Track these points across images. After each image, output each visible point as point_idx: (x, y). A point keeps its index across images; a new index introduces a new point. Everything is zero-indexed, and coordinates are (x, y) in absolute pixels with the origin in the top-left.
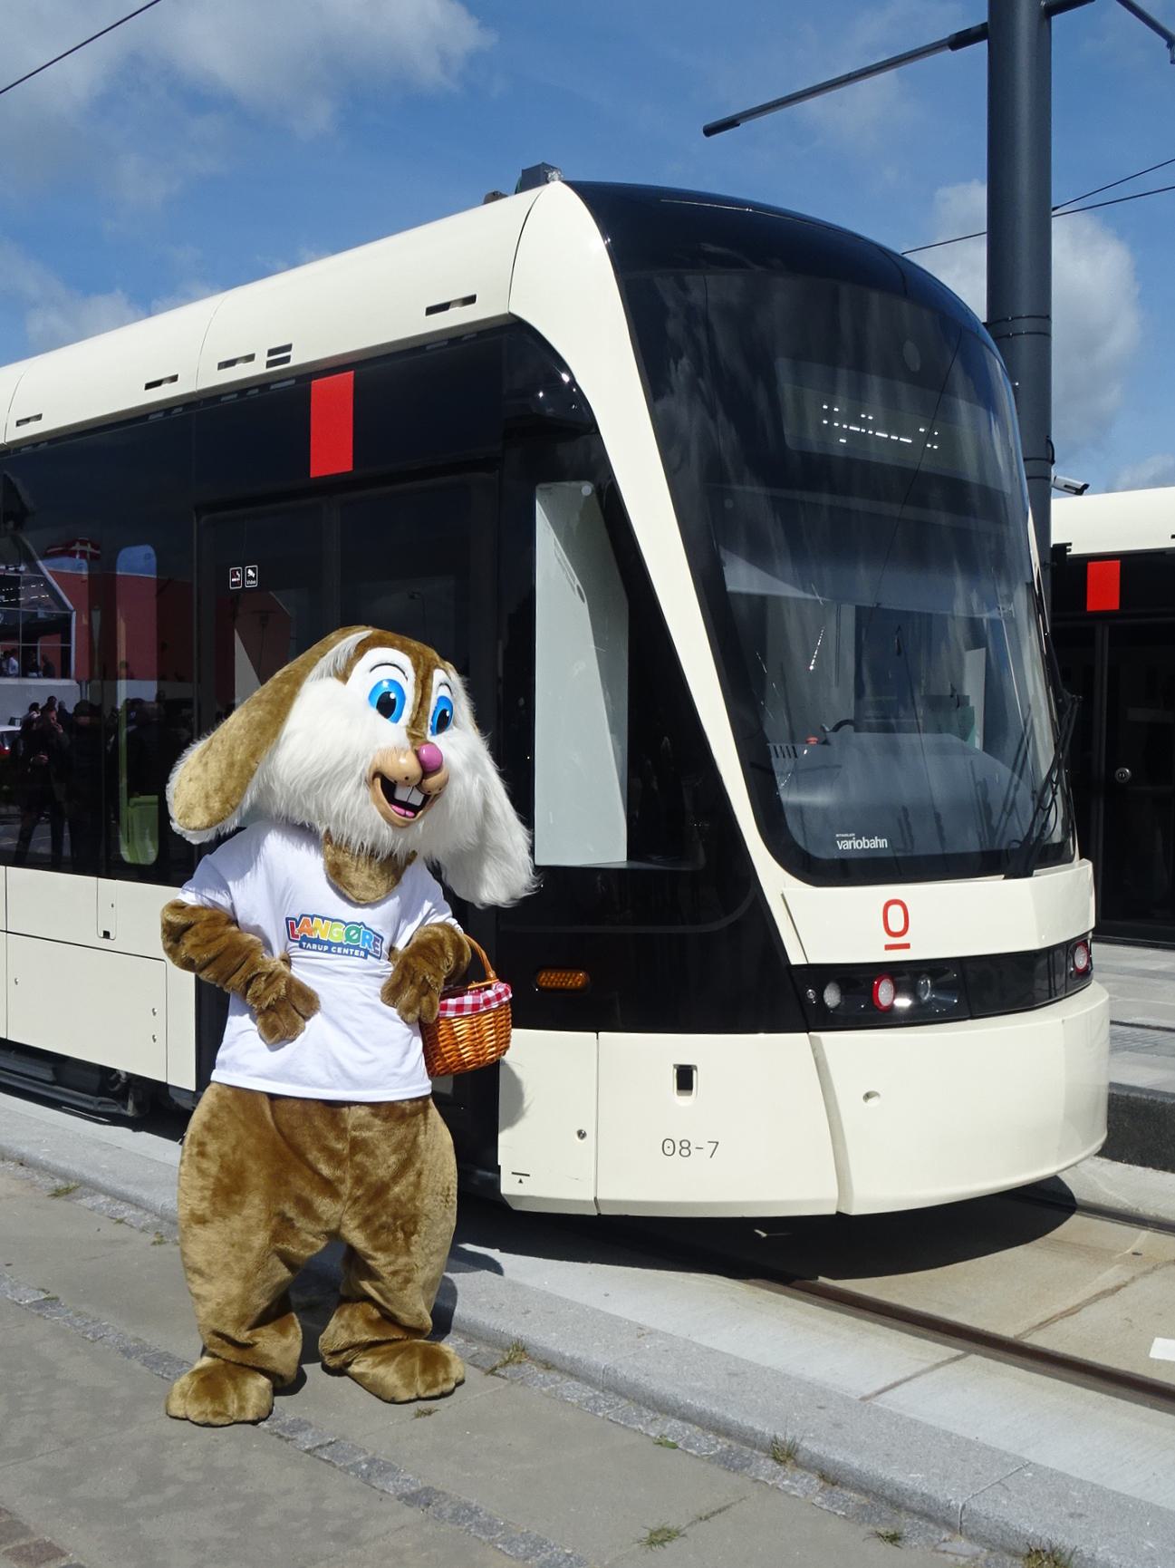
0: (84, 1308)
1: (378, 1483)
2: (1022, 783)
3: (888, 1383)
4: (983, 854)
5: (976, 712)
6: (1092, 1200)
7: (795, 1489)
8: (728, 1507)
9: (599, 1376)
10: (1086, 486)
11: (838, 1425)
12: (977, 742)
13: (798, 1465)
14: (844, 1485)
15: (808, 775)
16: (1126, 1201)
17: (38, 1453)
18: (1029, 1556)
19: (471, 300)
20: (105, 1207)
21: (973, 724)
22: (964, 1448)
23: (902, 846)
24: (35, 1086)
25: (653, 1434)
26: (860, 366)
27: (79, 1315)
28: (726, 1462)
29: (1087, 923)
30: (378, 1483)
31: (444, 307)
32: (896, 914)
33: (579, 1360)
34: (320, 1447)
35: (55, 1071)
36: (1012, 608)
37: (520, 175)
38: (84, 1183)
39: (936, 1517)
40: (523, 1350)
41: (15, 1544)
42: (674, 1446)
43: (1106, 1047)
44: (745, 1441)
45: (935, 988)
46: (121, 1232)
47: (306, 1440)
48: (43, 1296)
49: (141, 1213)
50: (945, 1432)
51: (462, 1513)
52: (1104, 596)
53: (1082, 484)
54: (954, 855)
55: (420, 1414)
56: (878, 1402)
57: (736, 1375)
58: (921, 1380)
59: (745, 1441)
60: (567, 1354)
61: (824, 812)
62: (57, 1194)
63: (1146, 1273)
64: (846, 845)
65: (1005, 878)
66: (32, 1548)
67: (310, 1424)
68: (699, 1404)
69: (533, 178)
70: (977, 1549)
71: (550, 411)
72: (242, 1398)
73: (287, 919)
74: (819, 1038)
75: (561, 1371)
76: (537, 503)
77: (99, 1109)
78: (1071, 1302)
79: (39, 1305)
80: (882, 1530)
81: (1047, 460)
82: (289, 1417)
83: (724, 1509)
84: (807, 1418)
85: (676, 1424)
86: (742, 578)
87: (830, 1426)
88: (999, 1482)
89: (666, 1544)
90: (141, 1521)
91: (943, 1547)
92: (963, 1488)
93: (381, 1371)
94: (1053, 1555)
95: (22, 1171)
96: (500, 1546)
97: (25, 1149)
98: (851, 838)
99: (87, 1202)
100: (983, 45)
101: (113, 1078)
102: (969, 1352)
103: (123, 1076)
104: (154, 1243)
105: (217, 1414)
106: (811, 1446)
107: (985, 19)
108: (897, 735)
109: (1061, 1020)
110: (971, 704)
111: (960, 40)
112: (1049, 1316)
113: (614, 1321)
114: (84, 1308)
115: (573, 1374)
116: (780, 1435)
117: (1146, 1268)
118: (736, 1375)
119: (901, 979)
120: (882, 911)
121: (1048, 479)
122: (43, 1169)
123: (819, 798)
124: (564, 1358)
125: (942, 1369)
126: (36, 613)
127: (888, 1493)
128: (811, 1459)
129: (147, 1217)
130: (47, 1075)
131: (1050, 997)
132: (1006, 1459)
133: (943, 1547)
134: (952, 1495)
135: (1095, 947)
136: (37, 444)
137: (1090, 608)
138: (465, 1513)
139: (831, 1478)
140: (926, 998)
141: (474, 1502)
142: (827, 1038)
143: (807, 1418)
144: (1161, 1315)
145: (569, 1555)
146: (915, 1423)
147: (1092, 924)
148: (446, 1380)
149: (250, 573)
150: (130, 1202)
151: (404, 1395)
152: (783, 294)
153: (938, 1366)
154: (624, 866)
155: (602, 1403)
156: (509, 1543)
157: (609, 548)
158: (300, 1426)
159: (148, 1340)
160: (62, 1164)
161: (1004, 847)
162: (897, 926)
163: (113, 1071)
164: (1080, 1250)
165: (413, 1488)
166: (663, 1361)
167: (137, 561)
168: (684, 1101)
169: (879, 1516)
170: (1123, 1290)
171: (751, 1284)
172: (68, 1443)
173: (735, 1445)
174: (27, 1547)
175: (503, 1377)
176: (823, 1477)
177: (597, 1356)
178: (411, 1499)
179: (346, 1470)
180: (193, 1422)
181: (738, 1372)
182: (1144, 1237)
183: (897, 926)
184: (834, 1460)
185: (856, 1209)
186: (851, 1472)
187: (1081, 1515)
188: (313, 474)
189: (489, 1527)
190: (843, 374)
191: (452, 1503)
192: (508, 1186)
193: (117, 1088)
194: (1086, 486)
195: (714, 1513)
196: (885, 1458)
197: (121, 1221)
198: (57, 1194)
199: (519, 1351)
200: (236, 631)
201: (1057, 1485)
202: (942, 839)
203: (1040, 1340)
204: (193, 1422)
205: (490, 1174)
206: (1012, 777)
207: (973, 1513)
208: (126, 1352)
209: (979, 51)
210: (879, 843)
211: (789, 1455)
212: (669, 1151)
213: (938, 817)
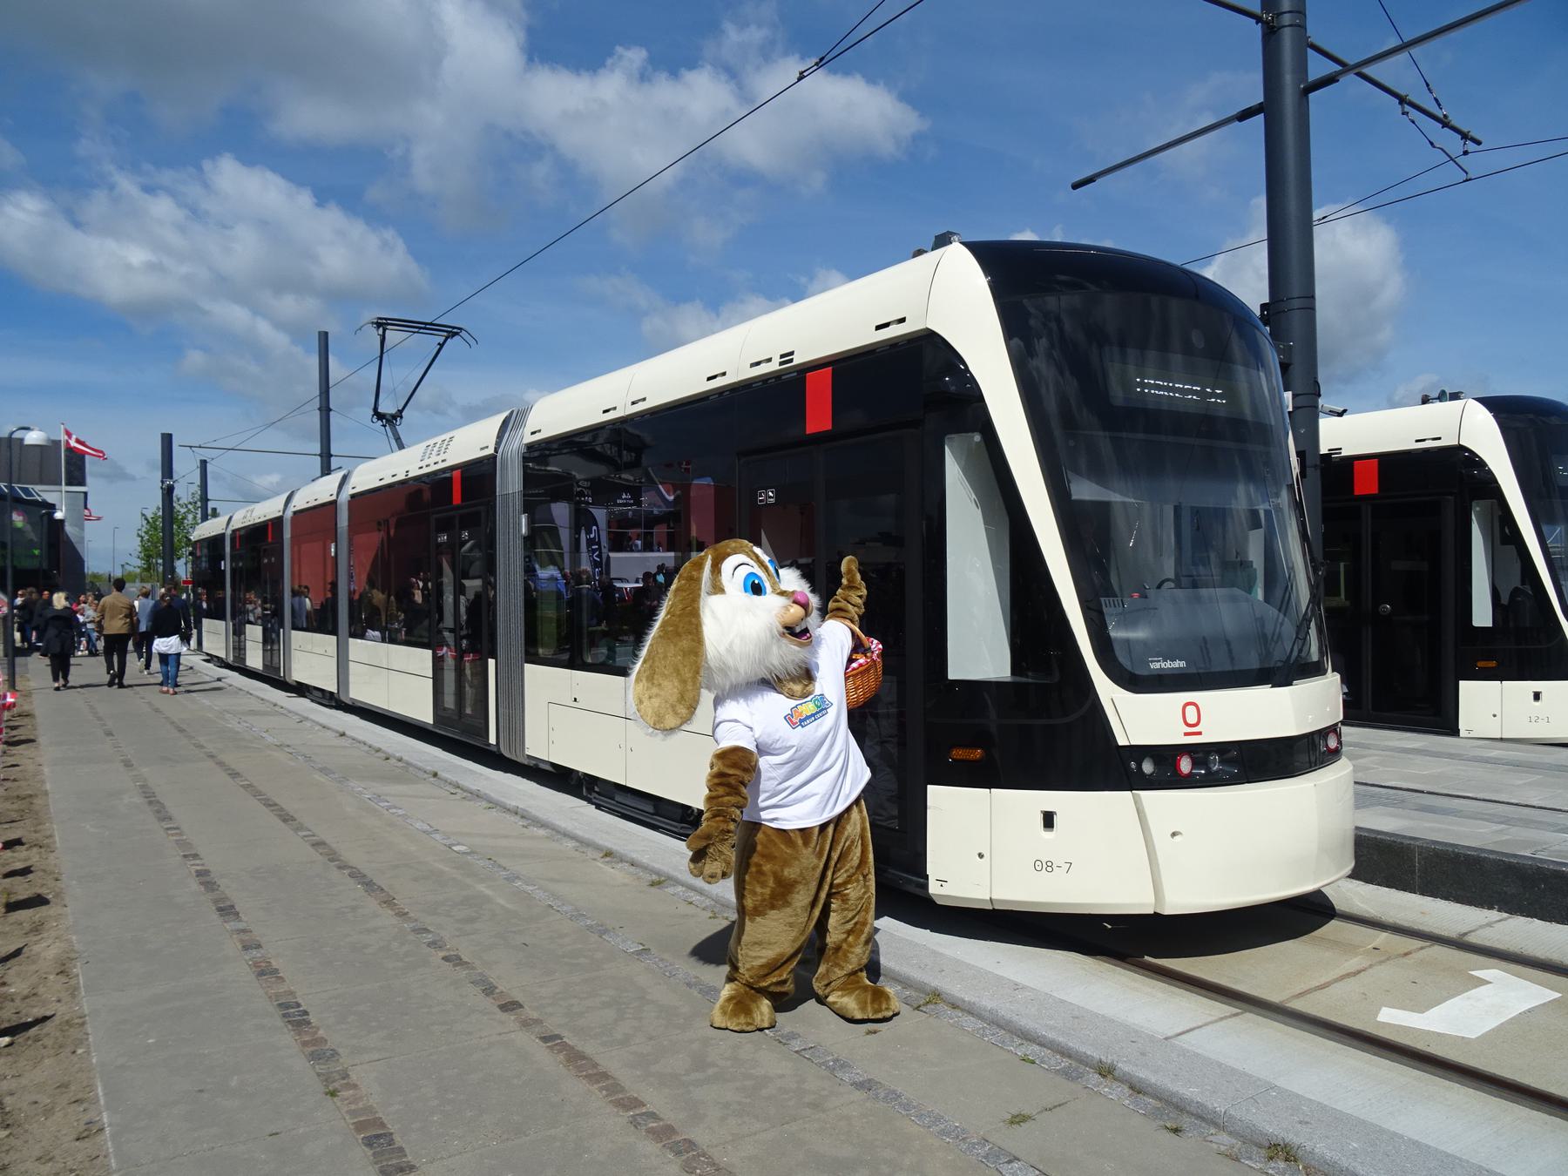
0: (666, 956)
1: (839, 1074)
2: (1286, 619)
3: (1185, 1029)
4: (1261, 670)
5: (1258, 572)
6: (1347, 910)
7: (1112, 1094)
8: (1066, 1103)
9: (987, 1014)
10: (1345, 411)
11: (1143, 1054)
12: (1259, 593)
13: (1115, 1079)
14: (1145, 1094)
15: (1128, 621)
16: (1372, 911)
17: (633, 1043)
18: (1270, 1148)
19: (902, 320)
20: (681, 894)
21: (1256, 579)
22: (1228, 1073)
23: (1203, 666)
24: (644, 816)
25: (1019, 1054)
26: (1164, 347)
27: (662, 960)
28: (1066, 1074)
29: (1339, 716)
30: (839, 1074)
31: (886, 325)
32: (1191, 711)
33: (974, 1004)
34: (805, 1049)
35: (655, 807)
36: (1279, 501)
37: (934, 239)
38: (669, 878)
39: (1207, 1118)
40: (938, 995)
41: (616, 1097)
42: (1033, 1062)
43: (1352, 802)
44: (1081, 1061)
45: (1221, 762)
46: (691, 910)
47: (796, 1045)
48: (641, 947)
49: (703, 898)
50: (1217, 1062)
51: (891, 1097)
52: (1366, 484)
53: (1342, 409)
54: (1240, 671)
55: (869, 1032)
56: (1175, 1041)
57: (1077, 1018)
58: (1209, 1028)
59: (1081, 1061)
60: (966, 999)
61: (1144, 643)
62: (653, 884)
63: (1381, 962)
64: (1155, 666)
65: (1272, 687)
66: (626, 1100)
67: (800, 1036)
68: (1051, 1035)
69: (942, 241)
70: (1234, 1141)
71: (953, 388)
72: (762, 1014)
73: (785, 718)
74: (1139, 795)
75: (963, 1010)
76: (946, 448)
77: (681, 831)
78: (1323, 980)
79: (638, 953)
80: (1168, 1125)
81: (1314, 394)
82: (787, 1030)
83: (1063, 1104)
84: (1123, 1048)
85: (1036, 1048)
86: (1084, 490)
87: (1138, 1054)
88: (1252, 1098)
89: (1022, 1124)
90: (691, 1088)
91: (1210, 1138)
92: (1226, 1099)
93: (845, 1000)
94: (1285, 1147)
95: (632, 869)
96: (913, 1118)
97: (634, 856)
98: (1159, 661)
99: (671, 890)
100: (1260, 118)
101: (689, 812)
102: (1246, 1011)
103: (696, 811)
104: (710, 918)
105: (748, 1024)
106: (1124, 1067)
107: (1262, 100)
108: (1200, 590)
109: (1313, 785)
110: (1254, 566)
111: (1245, 115)
112: (1306, 989)
113: (1000, 978)
114: (666, 956)
115: (970, 1013)
116: (1103, 1059)
117: (1383, 958)
118: (1077, 1018)
119: (1196, 756)
120: (1181, 712)
121: (1317, 407)
122: (645, 868)
123: (1139, 634)
124: (964, 1001)
125: (1225, 1021)
126: (652, 511)
127: (1175, 1100)
128: (1124, 1075)
129: (707, 901)
130: (650, 809)
131: (1311, 767)
132: (1258, 1083)
133: (1210, 1138)
134: (1218, 1104)
135: (1345, 730)
136: (643, 416)
137: (1357, 492)
138: (892, 1096)
139: (1137, 1089)
140: (1215, 769)
141: (899, 1090)
142: (1145, 795)
143: (1123, 1048)
144: (1388, 991)
145: (957, 1127)
146: (1197, 1055)
147: (1341, 718)
148: (887, 1009)
149: (771, 494)
150: (696, 891)
151: (859, 1016)
152: (1109, 307)
153: (1222, 1019)
154: (1009, 680)
155: (988, 1032)
156: (920, 1116)
157: (993, 476)
158: (793, 1036)
159: (702, 978)
160: (657, 866)
161: (1272, 666)
162: (1192, 719)
163: (690, 807)
164: (1336, 944)
165: (861, 1079)
166: (1029, 1007)
167: (703, 484)
168: (1048, 835)
169: (1168, 1114)
170: (1362, 974)
171: (1097, 959)
172: (651, 1039)
173: (1074, 1064)
174: (622, 1099)
175: (925, 1012)
176: (1132, 1087)
177: (987, 1002)
178: (859, 1086)
179: (820, 1065)
180: (732, 1030)
181: (1079, 1016)
182: (1383, 936)
183: (1192, 719)
184: (1138, 1077)
185: (1167, 911)
186: (1150, 1085)
187: (1307, 1123)
188: (807, 433)
189: (907, 1107)
190: (1152, 354)
191: (885, 1090)
192: (934, 889)
193: (692, 818)
194: (1345, 411)
195: (1055, 1107)
196: (1174, 1077)
197: (691, 903)
198: (653, 884)
199: (936, 996)
200: (763, 533)
201: (1293, 1102)
202: (1232, 659)
203: (1299, 1005)
204: (732, 1030)
205: (922, 880)
206: (1278, 616)
207: (1231, 1117)
208: (689, 985)
209: (1260, 119)
210: (1179, 664)
211: (1109, 1072)
212: (1039, 868)
213: (1228, 643)
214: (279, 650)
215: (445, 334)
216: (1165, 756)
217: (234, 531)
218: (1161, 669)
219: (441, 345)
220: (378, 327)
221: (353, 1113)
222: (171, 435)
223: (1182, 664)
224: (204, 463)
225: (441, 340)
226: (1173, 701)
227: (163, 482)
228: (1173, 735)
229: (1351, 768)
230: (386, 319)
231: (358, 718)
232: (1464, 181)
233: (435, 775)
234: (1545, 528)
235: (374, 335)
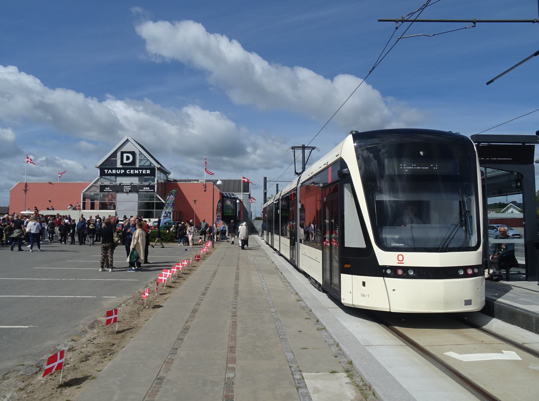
214: (295, 249)
215: (311, 149)
218: (401, 246)
219: (311, 152)
220: (293, 149)
221: (236, 335)
222: (266, 178)
224: (277, 185)
225: (310, 151)
227: (264, 191)
228: (395, 263)
229: (253, 236)
230: (294, 147)
231: (293, 267)
233: (282, 273)
234: (108, 208)
235: (291, 151)
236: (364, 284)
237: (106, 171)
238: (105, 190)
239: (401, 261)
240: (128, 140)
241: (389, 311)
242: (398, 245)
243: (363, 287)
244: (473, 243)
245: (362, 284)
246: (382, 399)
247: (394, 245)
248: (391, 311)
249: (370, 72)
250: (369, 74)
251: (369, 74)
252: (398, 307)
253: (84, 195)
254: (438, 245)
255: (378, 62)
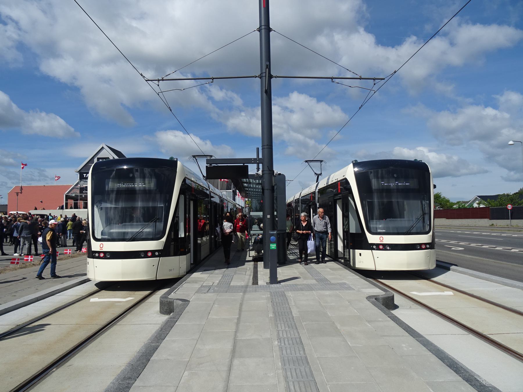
32: (102, 245)
162: (101, 247)
216: (378, 245)
217: (319, 190)
223: (385, 231)
226: (378, 236)
232: (375, 93)
236: (360, 254)
237: (85, 175)
238: (84, 192)
239: (381, 241)
240: (103, 147)
241: (375, 270)
242: (381, 231)
243: (360, 256)
244: (427, 229)
245: (359, 254)
246: (150, 338)
247: (379, 231)
248: (377, 270)
249: (360, 108)
250: (360, 109)
251: (360, 109)
252: (381, 267)
253: (66, 196)
254: (405, 231)
255: (365, 101)
